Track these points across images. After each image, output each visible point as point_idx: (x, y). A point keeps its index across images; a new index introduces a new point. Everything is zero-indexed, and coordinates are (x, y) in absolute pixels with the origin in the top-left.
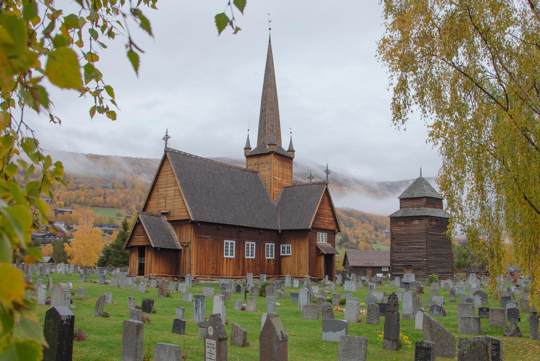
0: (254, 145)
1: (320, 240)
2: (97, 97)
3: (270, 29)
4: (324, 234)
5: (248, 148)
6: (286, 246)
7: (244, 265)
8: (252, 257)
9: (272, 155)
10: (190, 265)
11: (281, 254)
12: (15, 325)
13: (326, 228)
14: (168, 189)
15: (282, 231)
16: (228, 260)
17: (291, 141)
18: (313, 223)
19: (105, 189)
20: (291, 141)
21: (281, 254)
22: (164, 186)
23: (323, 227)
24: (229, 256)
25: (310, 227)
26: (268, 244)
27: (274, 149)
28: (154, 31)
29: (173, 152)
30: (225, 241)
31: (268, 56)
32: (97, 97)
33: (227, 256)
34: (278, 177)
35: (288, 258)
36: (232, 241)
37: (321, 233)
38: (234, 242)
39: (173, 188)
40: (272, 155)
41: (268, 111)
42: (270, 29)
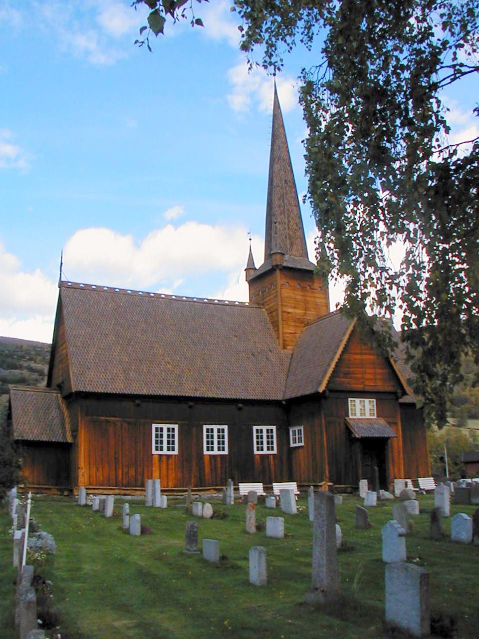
0: (259, 261)
2: (473, 69)
4: (367, 401)
5: (250, 268)
6: (296, 429)
7: (201, 469)
8: (221, 453)
9: (278, 272)
10: (176, 495)
11: (292, 445)
15: (287, 401)
16: (164, 459)
17: (251, 254)
20: (251, 254)
21: (292, 445)
27: (253, 267)
28: (152, 50)
29: (75, 287)
32: (473, 69)
35: (301, 451)
37: (357, 401)
40: (278, 272)
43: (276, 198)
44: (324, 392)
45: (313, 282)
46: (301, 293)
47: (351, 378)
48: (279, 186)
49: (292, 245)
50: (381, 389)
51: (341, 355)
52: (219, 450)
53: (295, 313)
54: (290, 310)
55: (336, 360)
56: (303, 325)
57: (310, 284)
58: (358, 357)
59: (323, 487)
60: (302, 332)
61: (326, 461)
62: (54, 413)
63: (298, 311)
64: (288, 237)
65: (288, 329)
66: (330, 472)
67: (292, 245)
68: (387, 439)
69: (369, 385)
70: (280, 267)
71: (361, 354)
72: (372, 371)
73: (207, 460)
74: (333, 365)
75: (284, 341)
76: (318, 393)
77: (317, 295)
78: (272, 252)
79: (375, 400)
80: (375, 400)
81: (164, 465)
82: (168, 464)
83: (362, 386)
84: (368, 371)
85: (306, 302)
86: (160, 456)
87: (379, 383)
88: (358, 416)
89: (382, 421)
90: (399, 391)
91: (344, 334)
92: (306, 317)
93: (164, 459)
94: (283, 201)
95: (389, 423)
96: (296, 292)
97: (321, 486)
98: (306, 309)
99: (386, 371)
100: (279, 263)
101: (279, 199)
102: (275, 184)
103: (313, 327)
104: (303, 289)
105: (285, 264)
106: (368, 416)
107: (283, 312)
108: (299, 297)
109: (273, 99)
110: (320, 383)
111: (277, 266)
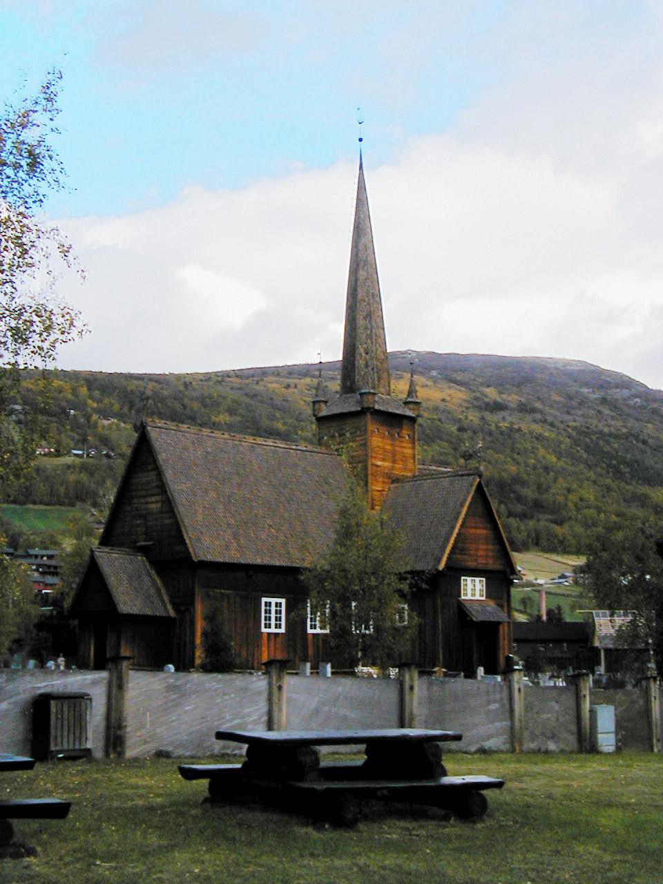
1: (469, 592)
3: (361, 140)
4: (477, 579)
7: (305, 647)
9: (369, 416)
12: (17, 861)
13: (480, 567)
14: (150, 500)
18: (449, 558)
19: (543, 419)
22: (143, 493)
23: (472, 564)
24: (273, 630)
25: (441, 567)
26: (268, 600)
30: (264, 600)
31: (358, 199)
33: (268, 630)
34: (383, 460)
36: (279, 600)
37: (469, 579)
38: (283, 601)
39: (158, 498)
40: (369, 416)
41: (361, 322)
42: (361, 140)
43: (361, 317)
44: (443, 569)
45: (402, 428)
46: (390, 442)
47: (465, 554)
48: (364, 301)
49: (379, 379)
50: (491, 567)
51: (460, 530)
52: (270, 603)
53: (384, 467)
54: (379, 463)
55: (455, 535)
56: (390, 481)
57: (398, 430)
58: (473, 531)
59: (438, 674)
60: (389, 489)
61: (441, 646)
62: (146, 579)
63: (386, 464)
64: (375, 370)
65: (377, 486)
66: (443, 657)
67: (379, 379)
68: (498, 624)
69: (481, 563)
70: (372, 410)
71: (475, 528)
72: (484, 547)
73: (310, 637)
74: (452, 541)
75: (372, 500)
76: (439, 572)
77: (404, 445)
78: (409, 400)
79: (484, 579)
80: (484, 579)
81: (272, 644)
82: (275, 644)
83: (475, 564)
84: (481, 547)
85: (394, 454)
86: (269, 634)
87: (491, 561)
88: (469, 597)
89: (492, 604)
90: (508, 570)
91: (462, 505)
92: (394, 472)
93: (272, 637)
94: (370, 321)
95: (498, 605)
96: (385, 441)
97: (435, 672)
98: (394, 462)
99: (497, 547)
100: (371, 406)
101: (365, 318)
102: (359, 297)
103: (407, 486)
104: (392, 437)
105: (377, 407)
106: (477, 597)
107: (373, 465)
108: (388, 447)
109: (357, 175)
110: (439, 560)
111: (369, 408)
